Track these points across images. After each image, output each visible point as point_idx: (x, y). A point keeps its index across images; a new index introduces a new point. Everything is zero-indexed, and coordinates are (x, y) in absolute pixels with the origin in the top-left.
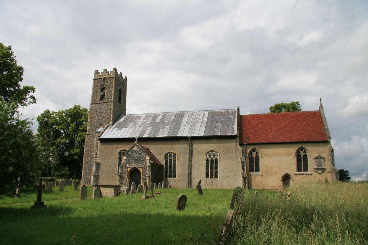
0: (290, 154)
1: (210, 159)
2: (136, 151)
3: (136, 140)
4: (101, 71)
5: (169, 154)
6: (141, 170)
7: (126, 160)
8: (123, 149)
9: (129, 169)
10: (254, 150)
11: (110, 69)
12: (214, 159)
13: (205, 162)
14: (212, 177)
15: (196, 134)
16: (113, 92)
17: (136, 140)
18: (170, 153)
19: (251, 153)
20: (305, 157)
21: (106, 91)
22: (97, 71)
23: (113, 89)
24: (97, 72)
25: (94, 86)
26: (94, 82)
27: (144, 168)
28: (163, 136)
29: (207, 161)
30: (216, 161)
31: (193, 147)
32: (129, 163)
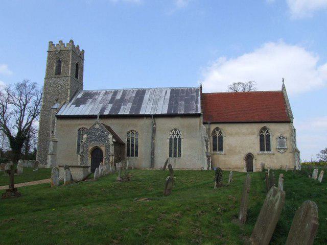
0: (253, 134)
1: (173, 138)
2: (98, 128)
3: (98, 117)
4: (56, 42)
5: (81, 130)
6: (103, 149)
7: (87, 139)
8: (82, 127)
9: (91, 148)
10: (217, 129)
11: (66, 42)
12: (178, 138)
13: (168, 141)
14: (175, 156)
15: (159, 112)
16: (70, 66)
17: (98, 117)
18: (132, 131)
19: (214, 132)
20: (268, 137)
21: (62, 65)
22: (52, 42)
23: (70, 63)
24: (51, 44)
25: (49, 59)
26: (49, 55)
27: (108, 147)
28: (125, 114)
29: (171, 139)
30: (180, 139)
31: (156, 125)
32: (91, 141)
